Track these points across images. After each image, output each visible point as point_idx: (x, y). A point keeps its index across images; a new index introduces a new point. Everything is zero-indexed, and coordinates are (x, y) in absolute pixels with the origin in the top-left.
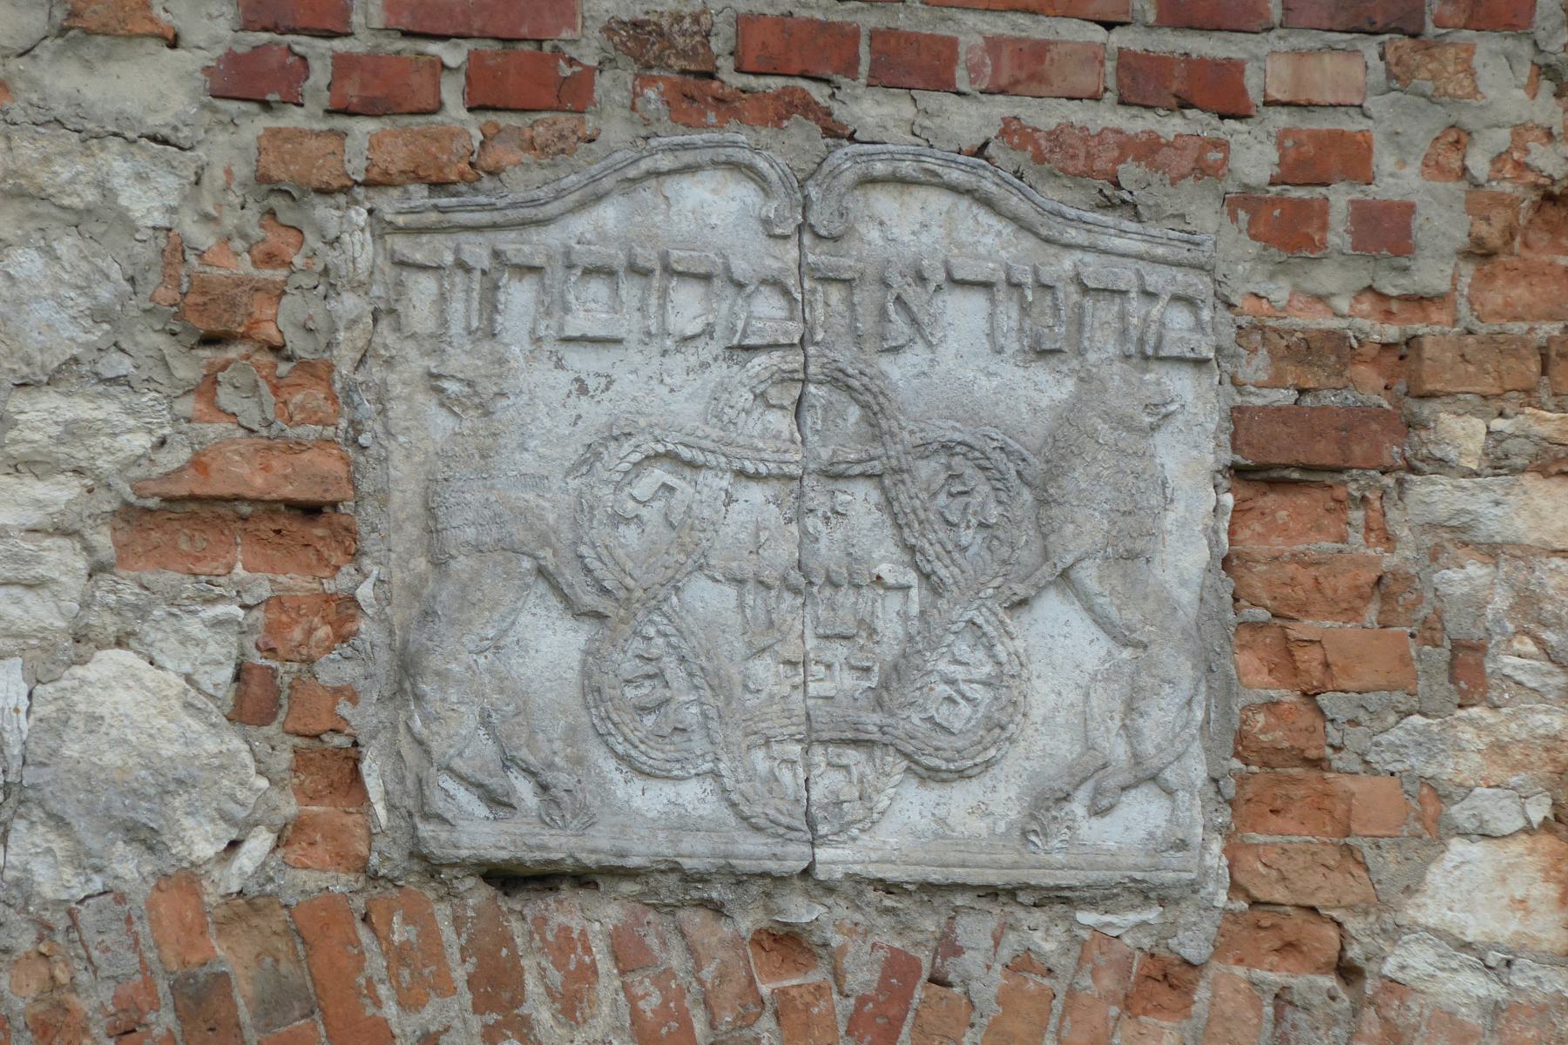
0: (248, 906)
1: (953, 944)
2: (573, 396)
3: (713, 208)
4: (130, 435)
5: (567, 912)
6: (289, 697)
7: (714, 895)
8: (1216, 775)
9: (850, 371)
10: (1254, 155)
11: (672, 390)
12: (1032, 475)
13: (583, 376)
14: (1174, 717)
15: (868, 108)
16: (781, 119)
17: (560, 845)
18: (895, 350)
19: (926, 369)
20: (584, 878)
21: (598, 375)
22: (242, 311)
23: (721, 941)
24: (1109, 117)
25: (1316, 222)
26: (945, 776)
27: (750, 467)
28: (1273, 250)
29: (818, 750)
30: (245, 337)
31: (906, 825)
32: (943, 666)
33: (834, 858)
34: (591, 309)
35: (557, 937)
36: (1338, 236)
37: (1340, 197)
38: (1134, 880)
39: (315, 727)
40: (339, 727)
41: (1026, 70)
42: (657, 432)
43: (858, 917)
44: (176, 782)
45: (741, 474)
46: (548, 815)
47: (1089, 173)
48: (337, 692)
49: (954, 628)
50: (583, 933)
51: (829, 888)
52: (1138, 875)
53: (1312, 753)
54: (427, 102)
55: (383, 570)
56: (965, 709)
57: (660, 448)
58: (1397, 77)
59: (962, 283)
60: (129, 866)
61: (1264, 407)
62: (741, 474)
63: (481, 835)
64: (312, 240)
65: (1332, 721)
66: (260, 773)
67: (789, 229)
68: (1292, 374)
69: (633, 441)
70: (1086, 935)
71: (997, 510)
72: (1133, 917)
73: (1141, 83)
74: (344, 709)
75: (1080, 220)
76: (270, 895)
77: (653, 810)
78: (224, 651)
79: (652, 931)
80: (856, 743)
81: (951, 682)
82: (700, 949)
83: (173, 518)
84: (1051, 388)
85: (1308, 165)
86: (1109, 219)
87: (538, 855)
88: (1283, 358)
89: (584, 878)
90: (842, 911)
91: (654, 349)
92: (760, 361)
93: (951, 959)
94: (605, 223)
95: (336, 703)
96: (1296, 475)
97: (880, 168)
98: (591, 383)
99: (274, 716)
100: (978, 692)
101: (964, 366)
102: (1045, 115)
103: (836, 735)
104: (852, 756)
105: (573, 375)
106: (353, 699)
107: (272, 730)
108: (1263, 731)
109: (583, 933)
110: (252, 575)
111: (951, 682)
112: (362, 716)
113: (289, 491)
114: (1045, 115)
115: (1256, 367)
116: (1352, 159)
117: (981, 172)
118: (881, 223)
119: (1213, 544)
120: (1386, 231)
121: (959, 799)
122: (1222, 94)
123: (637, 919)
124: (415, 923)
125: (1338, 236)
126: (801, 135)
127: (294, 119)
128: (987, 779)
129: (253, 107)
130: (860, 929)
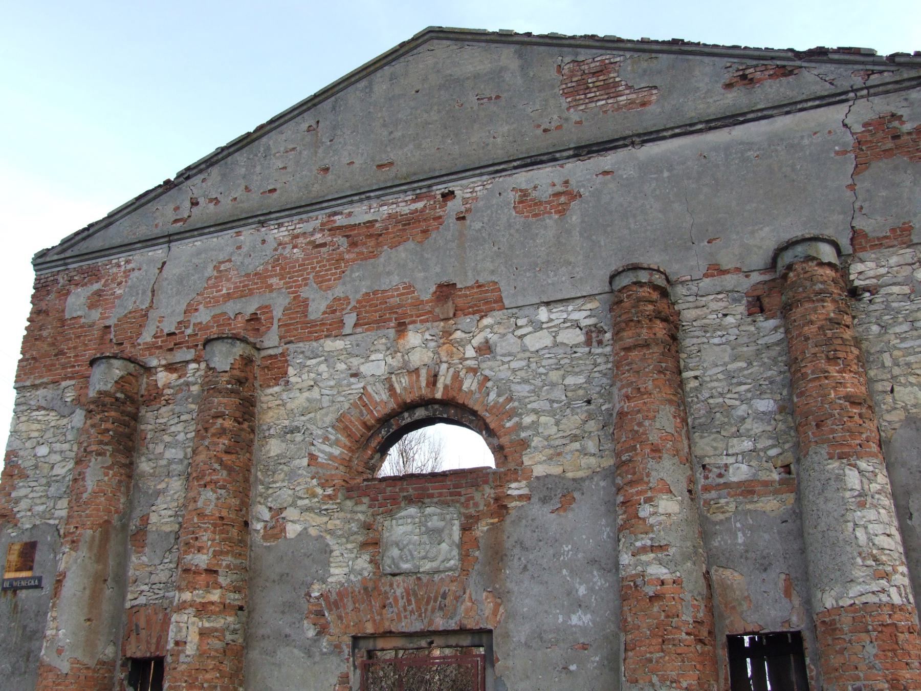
0: (370, 579)
3: (412, 510)
4: (361, 539)
5: (397, 578)
10: (463, 499)
12: (438, 531)
14: (455, 552)
15: (427, 501)
24: (449, 498)
31: (427, 566)
33: (421, 570)
34: (400, 522)
36: (471, 505)
37: (471, 502)
41: (441, 495)
42: (234, 532)
44: (363, 569)
46: (889, 555)
58: (477, 490)
60: (359, 577)
63: (388, 570)
71: (436, 535)
73: (451, 494)
77: (405, 566)
83: (364, 545)
84: (443, 523)
85: (468, 500)
94: (403, 513)
101: (435, 522)
102: (443, 498)
110: (371, 549)
112: (380, 562)
114: (443, 498)
115: (463, 519)
116: (472, 498)
120: (476, 505)
122: (459, 494)
125: (471, 505)
126: (420, 504)
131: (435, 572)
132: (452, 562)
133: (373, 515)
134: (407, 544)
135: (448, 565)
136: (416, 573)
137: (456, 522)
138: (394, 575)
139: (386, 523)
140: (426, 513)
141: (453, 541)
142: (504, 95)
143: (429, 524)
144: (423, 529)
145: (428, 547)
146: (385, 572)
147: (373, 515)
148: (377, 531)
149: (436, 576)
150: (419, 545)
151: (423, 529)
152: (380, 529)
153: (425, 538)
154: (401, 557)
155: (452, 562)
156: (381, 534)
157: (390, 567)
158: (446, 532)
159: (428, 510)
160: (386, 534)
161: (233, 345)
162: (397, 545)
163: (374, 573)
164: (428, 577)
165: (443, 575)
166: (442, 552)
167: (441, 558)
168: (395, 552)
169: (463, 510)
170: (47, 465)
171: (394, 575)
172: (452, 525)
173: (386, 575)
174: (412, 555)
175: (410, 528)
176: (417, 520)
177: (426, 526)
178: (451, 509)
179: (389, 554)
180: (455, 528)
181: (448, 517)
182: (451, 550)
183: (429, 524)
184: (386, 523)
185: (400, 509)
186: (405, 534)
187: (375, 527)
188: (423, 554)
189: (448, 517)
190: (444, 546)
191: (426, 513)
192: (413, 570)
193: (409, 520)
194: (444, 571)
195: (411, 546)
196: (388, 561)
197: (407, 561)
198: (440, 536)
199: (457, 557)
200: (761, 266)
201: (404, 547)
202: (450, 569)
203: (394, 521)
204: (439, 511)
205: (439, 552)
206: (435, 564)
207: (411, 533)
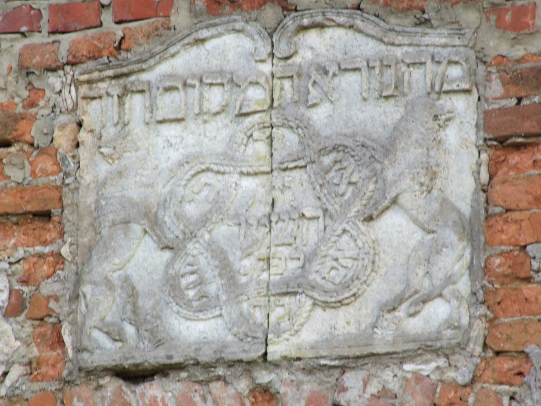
1: (343, 386)
2: (166, 149)
6: (30, 302)
7: (220, 373)
8: (474, 291)
9: (290, 118)
11: (210, 140)
12: (371, 152)
13: (169, 138)
14: (455, 258)
16: (261, 6)
17: (153, 357)
18: (314, 105)
19: (331, 113)
20: (162, 371)
21: (176, 137)
22: (10, 128)
23: (228, 395)
25: (530, 15)
26: (333, 305)
27: (245, 170)
28: (508, 32)
29: (272, 299)
30: (18, 141)
31: (308, 330)
32: (332, 252)
33: (276, 351)
34: (168, 104)
35: (150, 401)
38: (428, 346)
39: (40, 314)
40: (50, 313)
43: (293, 377)
45: (242, 174)
47: (410, 8)
48: (49, 298)
49: (336, 233)
50: (163, 399)
51: (276, 365)
52: (429, 343)
53: (523, 275)
54: (93, 21)
55: (73, 239)
56: (343, 271)
57: (203, 167)
59: (346, 70)
61: (499, 109)
62: (242, 174)
63: (106, 351)
64: (48, 93)
65: (534, 258)
66: (16, 339)
67: (264, 56)
68: (513, 90)
69: (190, 165)
70: (409, 376)
72: (433, 365)
74: (52, 304)
75: (404, 31)
76: (18, 395)
77: (194, 331)
78: (3, 285)
79: (197, 394)
80: (287, 294)
81: (336, 260)
82: (219, 401)
84: (390, 113)
86: (419, 29)
87: (130, 362)
88: (508, 84)
89: (162, 371)
90: (285, 375)
91: (200, 121)
92: (248, 121)
93: (342, 394)
94: (183, 61)
95: (48, 302)
96: (520, 140)
97: (306, 22)
98: (173, 141)
99: (22, 311)
100: (349, 263)
101: (348, 108)
103: (279, 291)
104: (286, 300)
105: (164, 139)
106: (57, 299)
107: (22, 317)
108: (499, 266)
109: (163, 399)
111: (336, 260)
112: (60, 308)
113: (29, 208)
115: (496, 88)
117: (354, 16)
118: (312, 48)
119: (477, 179)
121: (343, 314)
123: (190, 389)
124: (82, 401)
127: (36, 39)
128: (357, 304)
129: (18, 36)
130: (295, 383)
131: (347, 363)
132: (438, 311)
133: (25, 70)
134: (204, 221)
135: (415, 326)
136: (248, 366)
137: (464, 107)
138: (134, 375)
139: (92, 112)
140: (305, 56)
141: (445, 202)
142: (461, 402)
143: (319, 116)
144: (288, 140)
145: (311, 232)
146: (92, 360)
147: (25, 70)
148: (48, 150)
149: (352, 380)
150: (268, 221)
151: (288, 140)
152: (62, 141)
153: (297, 189)
154: (172, 285)
155: (438, 311)
156: (66, 168)
157: (117, 337)
158: (409, 155)
159: (316, 45)
160: (93, 169)
161: (375, 26)
162: (153, 224)
163: (32, 367)
164: (310, 385)
165: (389, 377)
166: (385, 260)
167: (378, 290)
168: (141, 259)
169: (497, 45)
170: (209, 81)
171: (134, 375)
172: (441, 120)
173: (91, 373)
174: (226, 270)
175: (216, 135)
176: (256, 95)
177: (302, 126)
178: (435, 38)
179: (104, 268)
180: (451, 135)
181: (418, 79)
182: (437, 248)
183: (319, 116)
184: (92, 112)
185: (166, 39)
186: (196, 165)
187: (34, 132)
188: (285, 266)
189: (418, 79)
190: (395, 227)
191: (305, 56)
192: (236, 352)
193: (215, 97)
194: (401, 358)
195: (223, 231)
196: (102, 305)
197: (204, 305)
198: (377, 176)
199: (464, 285)
200: (400, 197)
201: (191, 236)
202: (427, 348)
203: (136, 102)
204: (369, 48)
205: (370, 258)
206: (345, 323)
207: (228, 161)
